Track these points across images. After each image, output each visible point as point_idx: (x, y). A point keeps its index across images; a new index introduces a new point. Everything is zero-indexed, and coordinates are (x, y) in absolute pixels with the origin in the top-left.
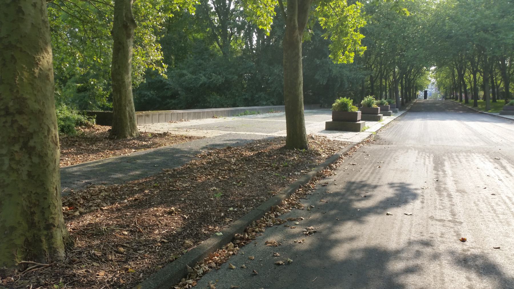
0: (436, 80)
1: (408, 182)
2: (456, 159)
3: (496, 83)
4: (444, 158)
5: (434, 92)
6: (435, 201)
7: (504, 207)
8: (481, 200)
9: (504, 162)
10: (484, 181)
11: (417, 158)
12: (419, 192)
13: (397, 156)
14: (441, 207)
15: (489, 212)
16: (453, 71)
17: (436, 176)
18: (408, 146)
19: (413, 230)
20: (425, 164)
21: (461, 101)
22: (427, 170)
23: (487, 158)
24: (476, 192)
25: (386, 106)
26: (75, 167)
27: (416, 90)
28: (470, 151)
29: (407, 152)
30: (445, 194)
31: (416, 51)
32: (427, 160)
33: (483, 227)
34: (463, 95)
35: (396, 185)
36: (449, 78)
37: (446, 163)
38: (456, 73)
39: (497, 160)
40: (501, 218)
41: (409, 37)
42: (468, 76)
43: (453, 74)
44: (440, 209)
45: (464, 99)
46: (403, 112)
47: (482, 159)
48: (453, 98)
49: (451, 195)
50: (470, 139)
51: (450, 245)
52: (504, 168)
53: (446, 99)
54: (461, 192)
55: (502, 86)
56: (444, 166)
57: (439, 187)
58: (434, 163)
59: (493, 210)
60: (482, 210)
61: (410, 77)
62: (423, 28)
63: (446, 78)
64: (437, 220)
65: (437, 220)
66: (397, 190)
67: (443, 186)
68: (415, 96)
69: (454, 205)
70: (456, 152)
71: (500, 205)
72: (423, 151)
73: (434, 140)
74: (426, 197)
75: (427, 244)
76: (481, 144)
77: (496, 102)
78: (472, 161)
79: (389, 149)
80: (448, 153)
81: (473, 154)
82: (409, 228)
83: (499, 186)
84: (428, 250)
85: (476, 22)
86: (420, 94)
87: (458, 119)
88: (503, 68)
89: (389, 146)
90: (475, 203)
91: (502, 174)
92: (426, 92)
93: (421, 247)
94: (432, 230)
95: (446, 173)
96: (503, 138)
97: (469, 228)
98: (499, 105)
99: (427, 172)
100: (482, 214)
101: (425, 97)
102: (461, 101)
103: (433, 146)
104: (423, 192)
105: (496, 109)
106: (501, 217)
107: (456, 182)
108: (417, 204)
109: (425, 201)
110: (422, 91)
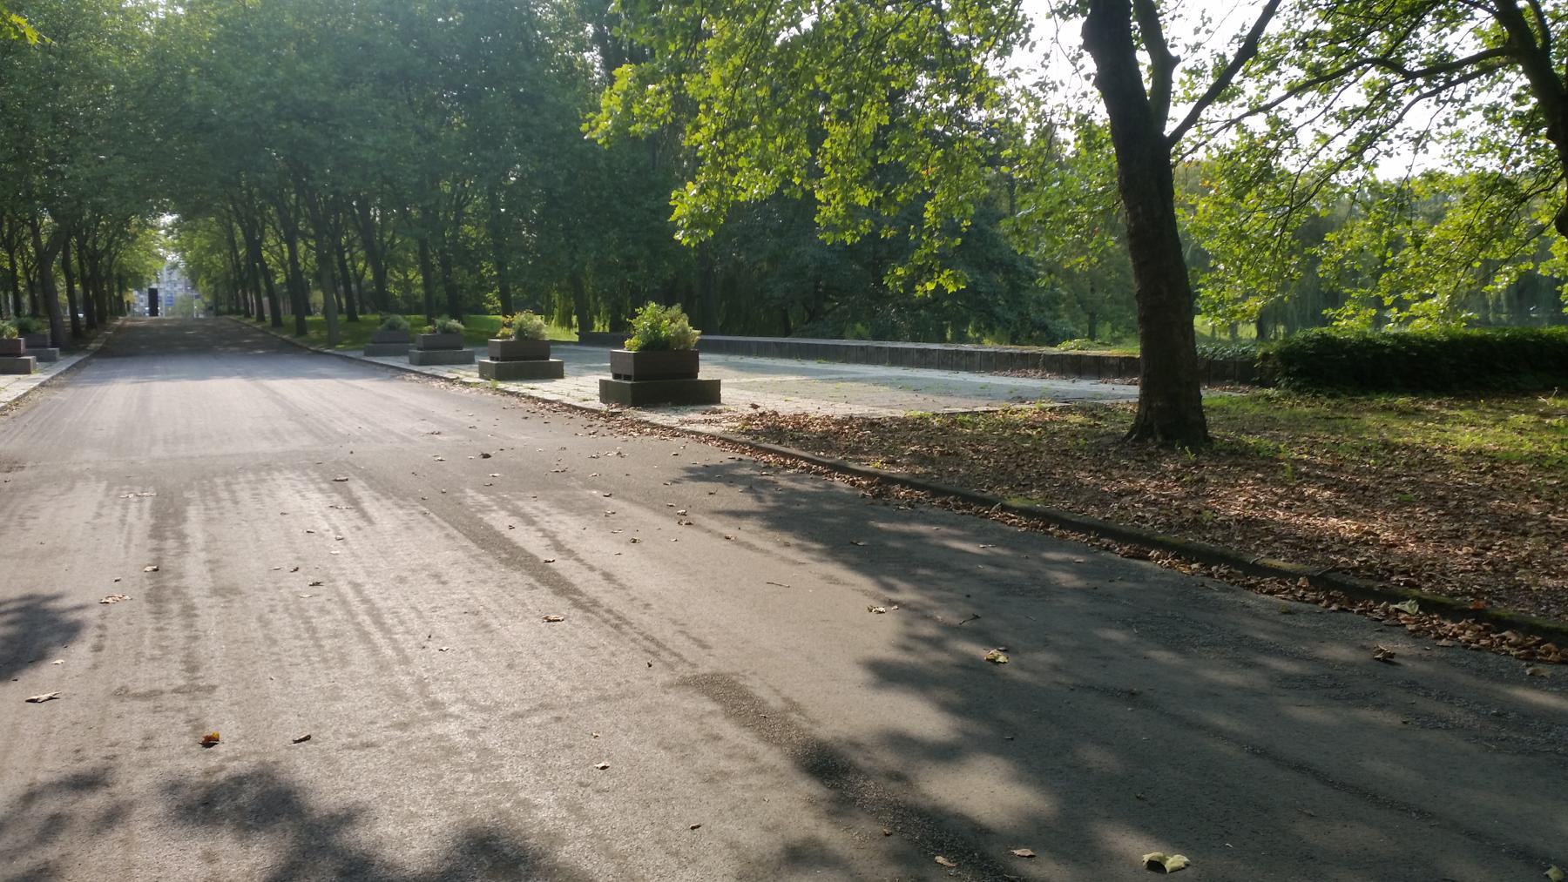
0: (183, 256)
1: (45, 590)
2: (224, 495)
3: (354, 267)
4: (186, 495)
5: (180, 294)
6: (141, 637)
7: (339, 614)
8: (280, 609)
9: (358, 487)
10: (295, 551)
11: (101, 505)
12: (92, 615)
13: (32, 508)
14: (157, 652)
15: (297, 637)
16: (231, 230)
17: (154, 555)
18: (75, 469)
19: (51, 748)
20: (123, 521)
21: (261, 318)
22: (129, 540)
23: (313, 481)
24: (270, 586)
25: (10, 341)
26: (791, 456)
27: (123, 288)
28: (269, 467)
29: (71, 489)
30: (175, 607)
31: (101, 162)
32: (133, 507)
33: (274, 686)
34: (265, 300)
35: (11, 606)
36: (220, 251)
37: (193, 513)
38: (239, 236)
39: (339, 483)
40: (327, 648)
41: (75, 116)
42: (273, 250)
43: (232, 241)
44: (153, 659)
45: (267, 315)
46: (75, 359)
47: (300, 486)
48: (238, 312)
49: (193, 608)
50: (275, 432)
51: (168, 765)
52: (355, 503)
53: (218, 313)
54: (225, 592)
55: (369, 276)
56: (185, 520)
57: (160, 589)
58: (152, 515)
59: (307, 630)
60: (279, 637)
61: (95, 242)
62: (119, 92)
63: (211, 251)
64: (137, 696)
65: (137, 696)
66: (12, 623)
67: (173, 584)
68: (121, 308)
69: (196, 638)
70: (226, 473)
71: (328, 613)
72: (119, 480)
73: (166, 442)
74: (112, 628)
75: (85, 783)
76: (305, 442)
77: (356, 320)
78: (271, 494)
79: (8, 485)
80: (204, 477)
81: (276, 474)
82: (35, 747)
83: (334, 558)
84: (96, 802)
85: (278, 91)
86: (137, 299)
87: (248, 375)
88: (366, 228)
89: (10, 476)
90: (260, 619)
91: (344, 521)
92: (153, 296)
93: (70, 799)
94: (114, 732)
95: (189, 540)
96: (366, 420)
97: (234, 698)
98: (364, 329)
99: (126, 547)
100: (276, 649)
101: (154, 312)
102: (259, 319)
103: (158, 460)
104: (103, 616)
105: (357, 339)
106: (327, 644)
107: (214, 565)
108: (80, 652)
109: (107, 643)
110: (139, 289)
